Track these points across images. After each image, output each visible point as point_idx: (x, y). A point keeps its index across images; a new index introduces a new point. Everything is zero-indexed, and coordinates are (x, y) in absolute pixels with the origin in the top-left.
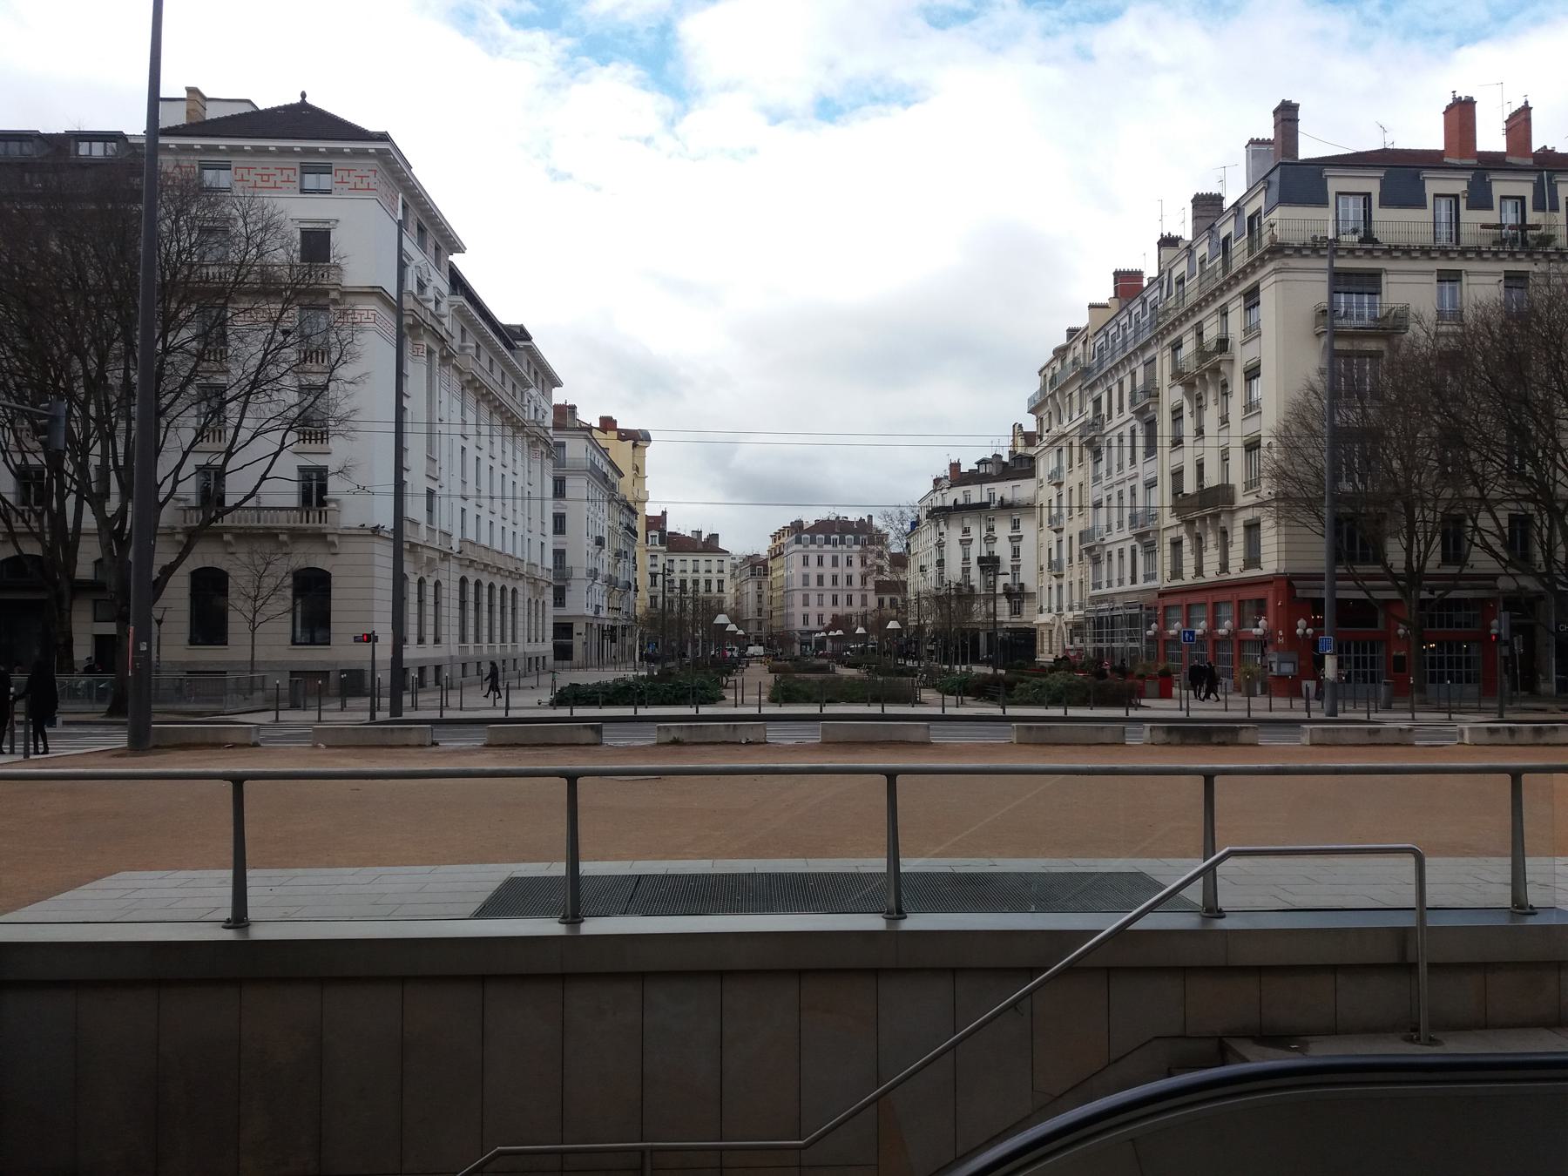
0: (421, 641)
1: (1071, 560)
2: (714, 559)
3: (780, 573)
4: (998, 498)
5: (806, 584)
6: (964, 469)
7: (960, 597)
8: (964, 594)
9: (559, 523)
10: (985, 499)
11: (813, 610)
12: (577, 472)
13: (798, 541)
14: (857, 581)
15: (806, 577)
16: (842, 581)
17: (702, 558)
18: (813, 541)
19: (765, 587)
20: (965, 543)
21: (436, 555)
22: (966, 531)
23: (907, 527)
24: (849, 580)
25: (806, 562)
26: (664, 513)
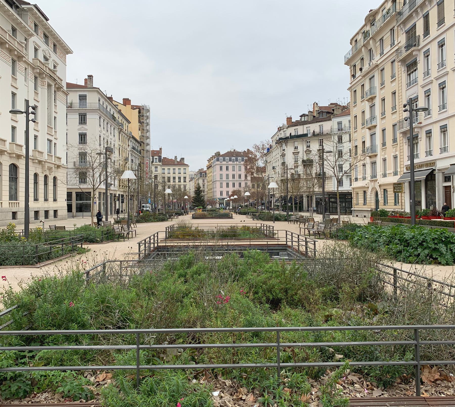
0: (46, 200)
1: (384, 144)
2: (182, 168)
3: (210, 174)
4: (312, 131)
5: (221, 178)
6: (294, 120)
7: (293, 180)
8: (296, 179)
9: (83, 138)
10: (305, 132)
11: (225, 189)
12: (93, 111)
13: (218, 160)
14: (243, 177)
15: (221, 175)
16: (237, 177)
17: (177, 168)
18: (224, 160)
19: (206, 181)
20: (296, 154)
21: (53, 166)
22: (296, 148)
23: (265, 152)
24: (240, 176)
25: (221, 168)
26: (161, 149)
